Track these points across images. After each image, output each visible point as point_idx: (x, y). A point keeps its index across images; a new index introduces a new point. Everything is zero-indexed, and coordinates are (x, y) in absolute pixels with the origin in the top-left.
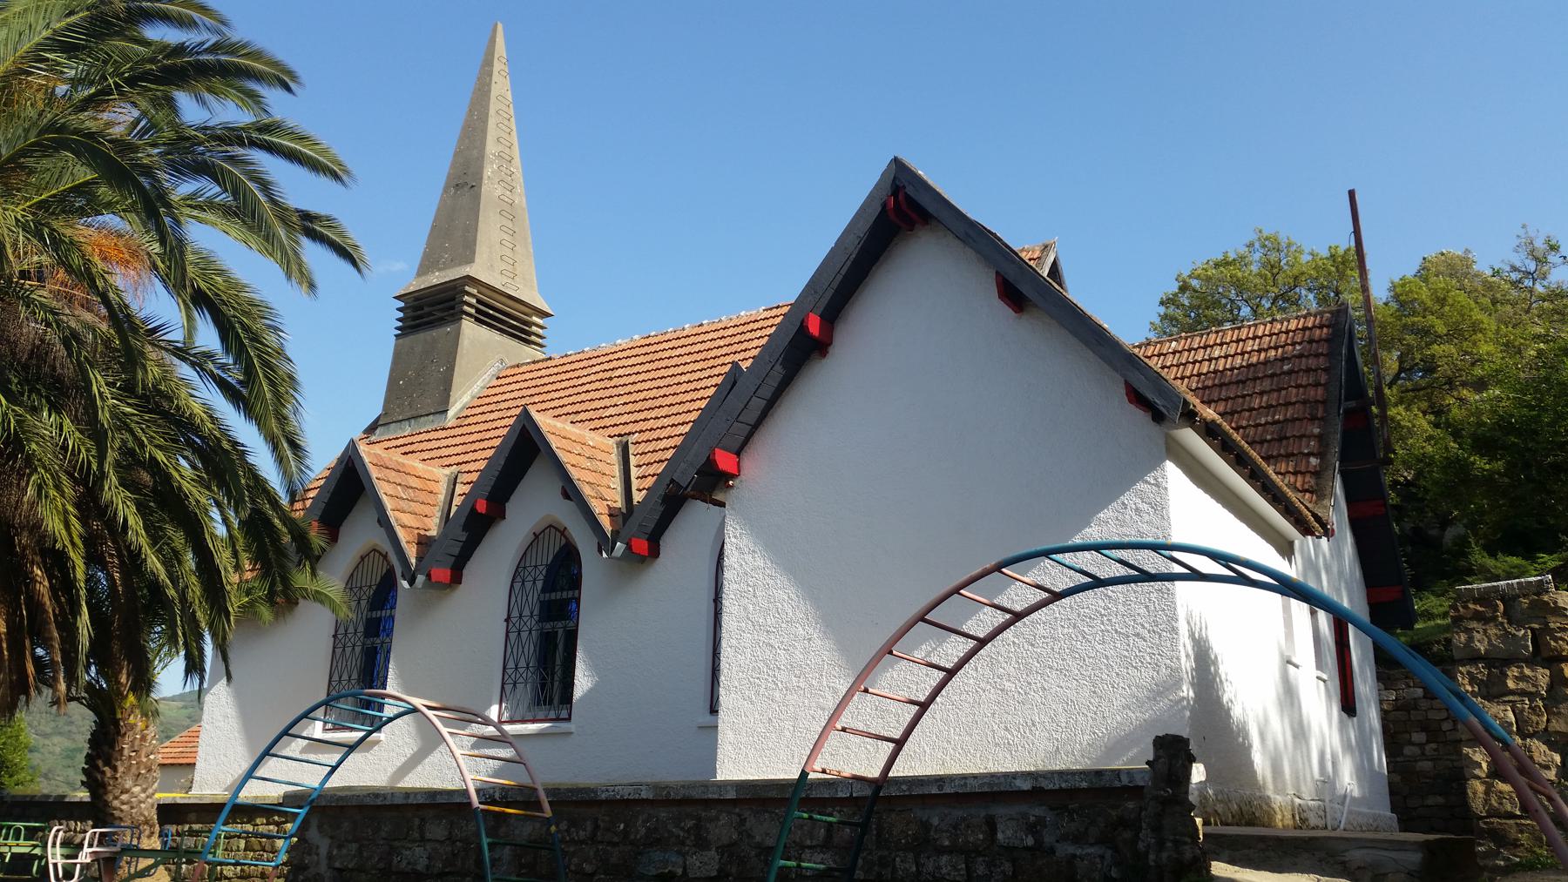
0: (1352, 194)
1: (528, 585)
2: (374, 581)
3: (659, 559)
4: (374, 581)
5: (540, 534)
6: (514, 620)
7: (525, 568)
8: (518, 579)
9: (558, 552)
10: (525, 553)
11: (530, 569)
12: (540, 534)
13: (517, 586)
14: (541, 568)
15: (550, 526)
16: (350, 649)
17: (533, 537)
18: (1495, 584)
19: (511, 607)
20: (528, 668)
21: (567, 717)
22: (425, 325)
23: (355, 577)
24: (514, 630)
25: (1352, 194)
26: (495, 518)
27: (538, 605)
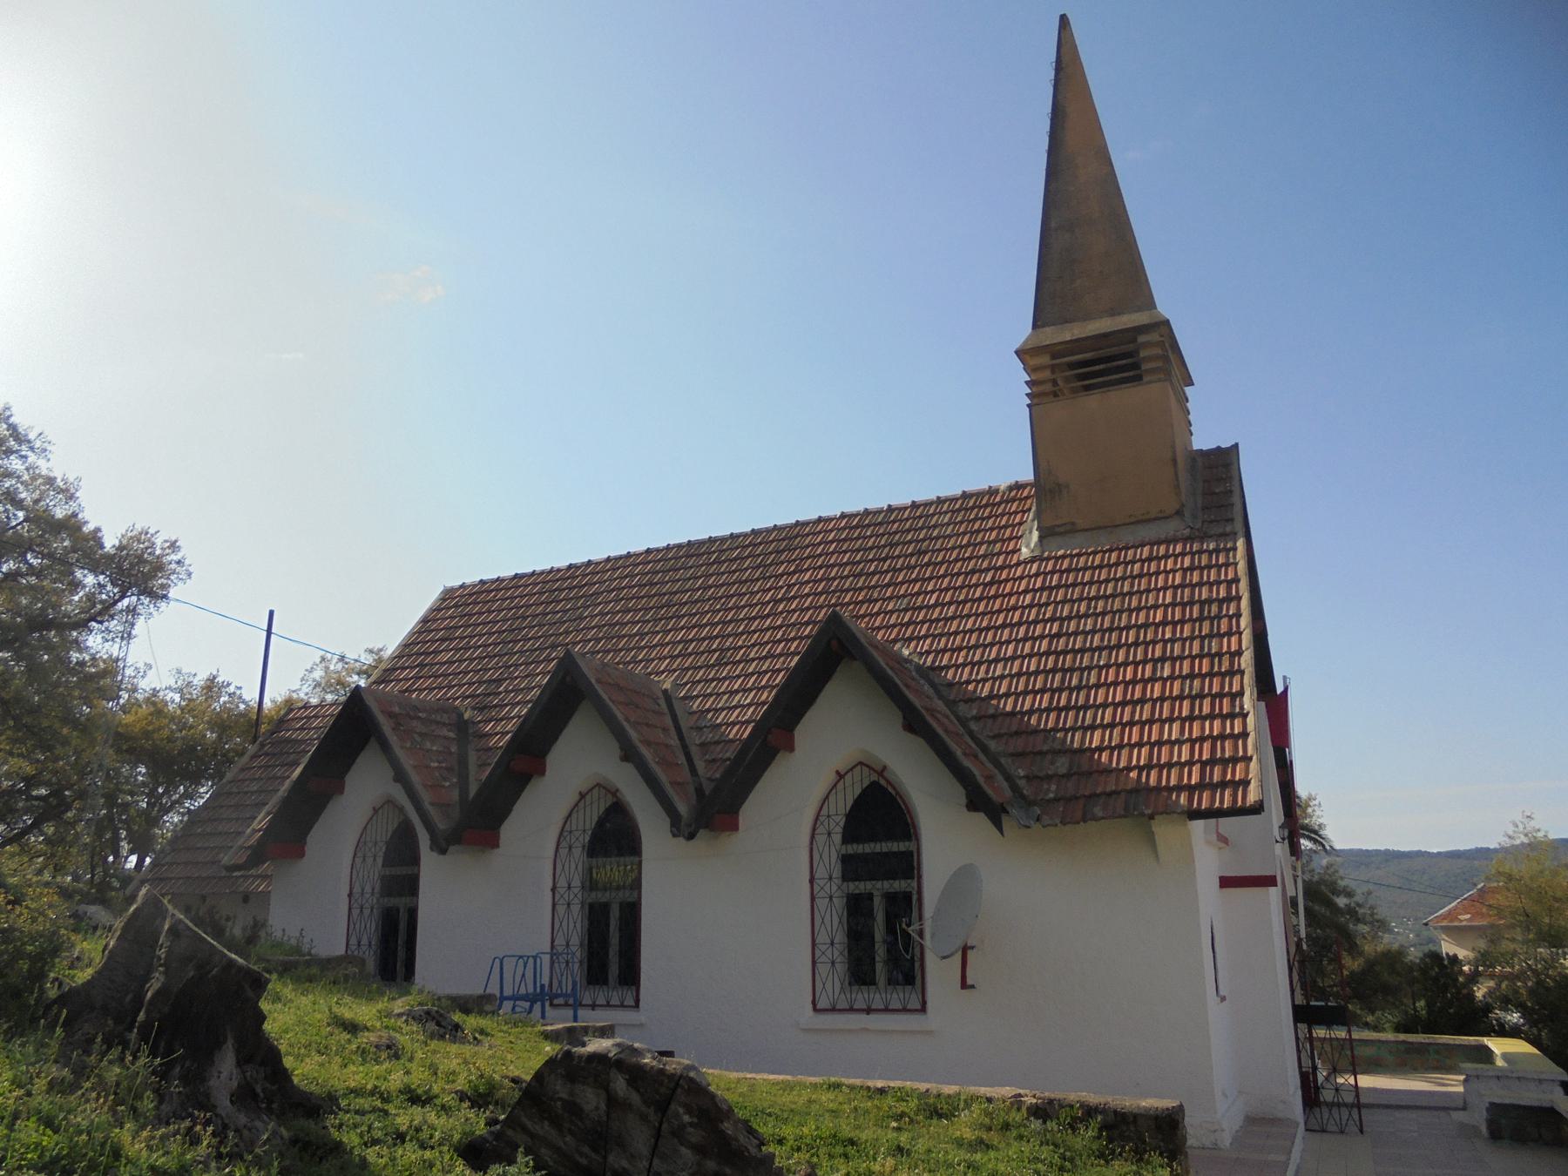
0: (271, 613)
1: (370, 861)
2: (588, 823)
3: (305, 859)
4: (588, 823)
5: (587, 793)
6: (562, 891)
7: (571, 832)
8: (564, 844)
9: (860, 796)
10: (365, 828)
11: (577, 834)
12: (587, 793)
13: (563, 852)
14: (838, 819)
15: (861, 763)
16: (358, 911)
17: (372, 812)
18: (226, 951)
19: (557, 876)
20: (832, 944)
21: (919, 1007)
22: (1113, 385)
23: (368, 832)
24: (822, 894)
25: (271, 613)
26: (532, 776)
27: (839, 866)
